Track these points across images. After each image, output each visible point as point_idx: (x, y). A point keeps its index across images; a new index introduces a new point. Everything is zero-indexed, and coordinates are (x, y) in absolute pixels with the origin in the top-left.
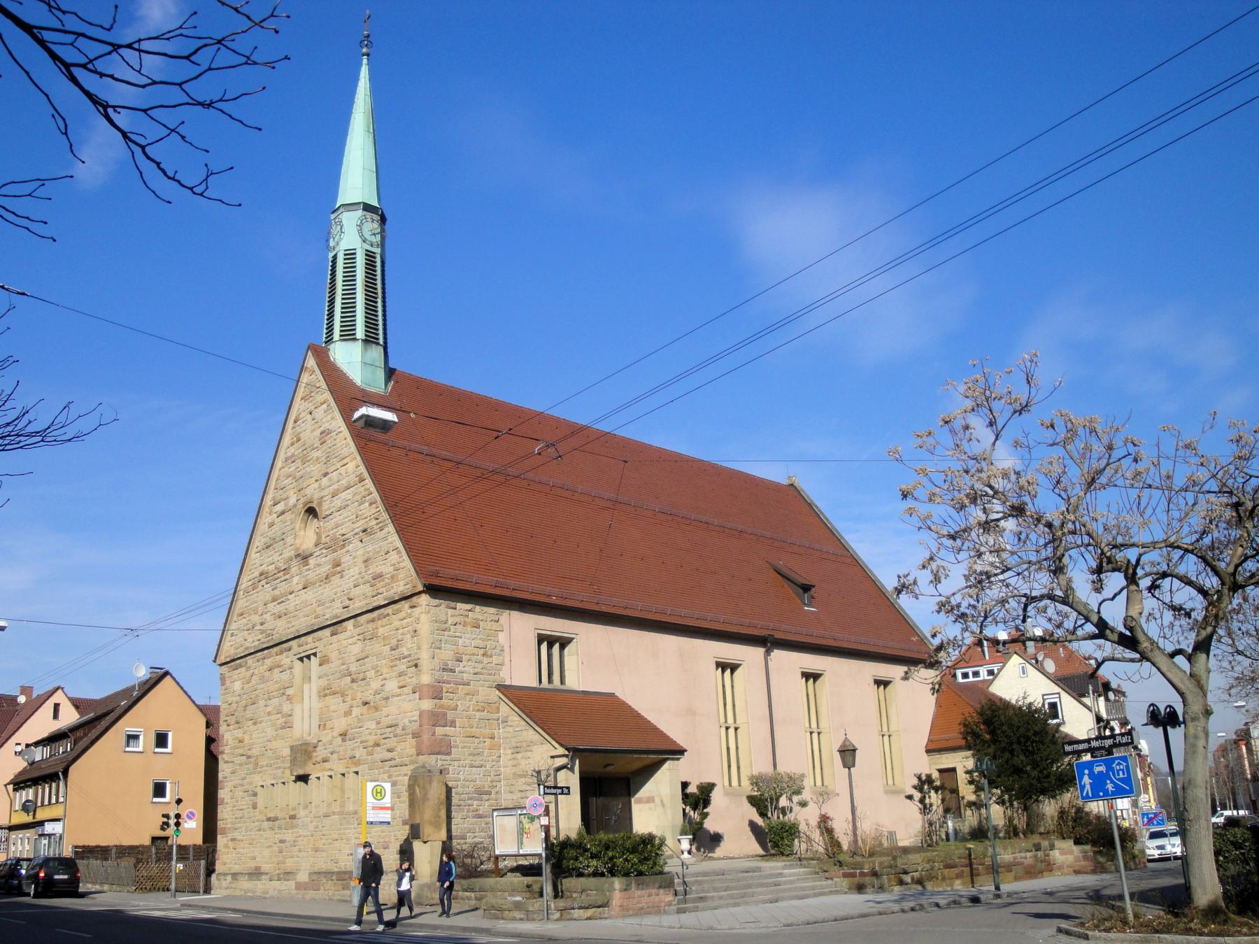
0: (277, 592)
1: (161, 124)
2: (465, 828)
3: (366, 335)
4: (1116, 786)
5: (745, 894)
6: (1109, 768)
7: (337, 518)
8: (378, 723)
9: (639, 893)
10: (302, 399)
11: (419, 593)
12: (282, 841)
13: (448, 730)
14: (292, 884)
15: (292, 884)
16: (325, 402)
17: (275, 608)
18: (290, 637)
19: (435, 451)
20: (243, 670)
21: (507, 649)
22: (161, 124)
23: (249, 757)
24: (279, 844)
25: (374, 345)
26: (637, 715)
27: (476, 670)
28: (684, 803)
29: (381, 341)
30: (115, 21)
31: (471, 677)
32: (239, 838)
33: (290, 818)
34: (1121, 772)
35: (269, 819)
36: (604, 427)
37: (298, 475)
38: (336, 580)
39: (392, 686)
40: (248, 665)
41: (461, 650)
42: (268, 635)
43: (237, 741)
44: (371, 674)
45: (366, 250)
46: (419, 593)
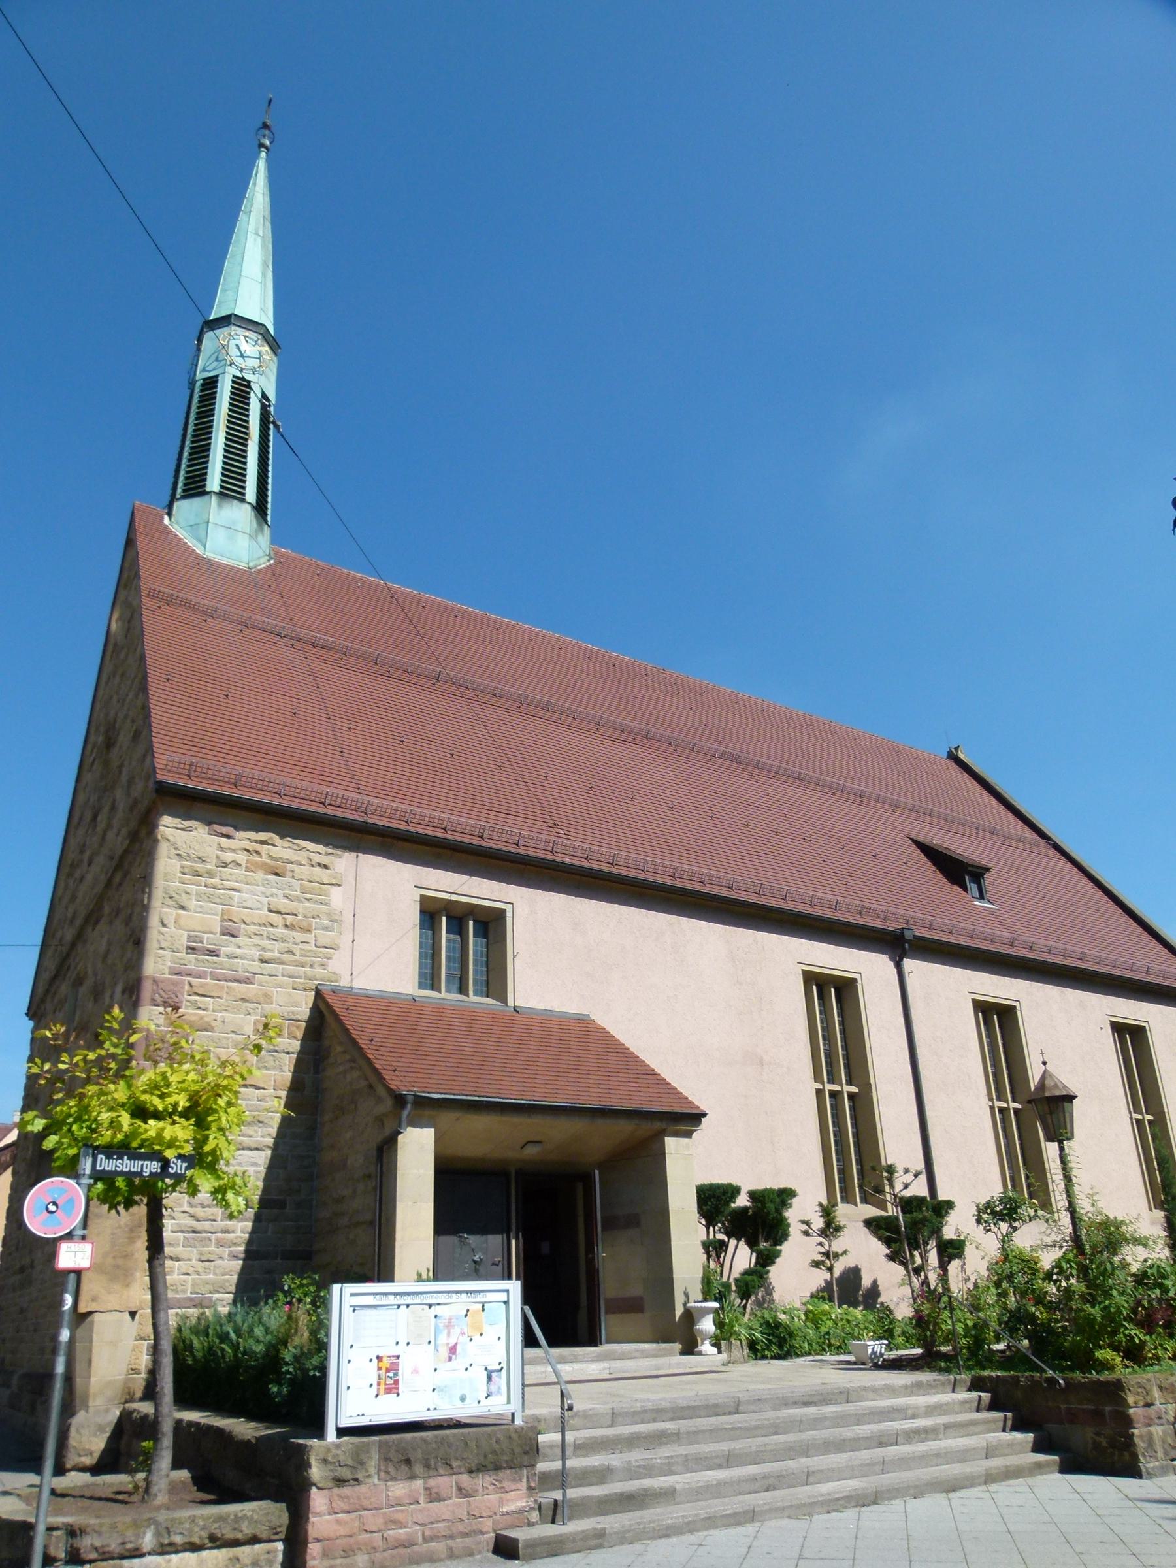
1: (284, 439)
3: (222, 487)
5: (780, 1477)
9: (399, 1489)
11: (1062, 1149)
21: (348, 918)
22: (284, 439)
25: (235, 502)
26: (622, 1051)
27: (267, 955)
28: (710, 1221)
29: (251, 494)
31: (256, 966)
41: (237, 913)
45: (234, 376)
46: (1062, 1149)
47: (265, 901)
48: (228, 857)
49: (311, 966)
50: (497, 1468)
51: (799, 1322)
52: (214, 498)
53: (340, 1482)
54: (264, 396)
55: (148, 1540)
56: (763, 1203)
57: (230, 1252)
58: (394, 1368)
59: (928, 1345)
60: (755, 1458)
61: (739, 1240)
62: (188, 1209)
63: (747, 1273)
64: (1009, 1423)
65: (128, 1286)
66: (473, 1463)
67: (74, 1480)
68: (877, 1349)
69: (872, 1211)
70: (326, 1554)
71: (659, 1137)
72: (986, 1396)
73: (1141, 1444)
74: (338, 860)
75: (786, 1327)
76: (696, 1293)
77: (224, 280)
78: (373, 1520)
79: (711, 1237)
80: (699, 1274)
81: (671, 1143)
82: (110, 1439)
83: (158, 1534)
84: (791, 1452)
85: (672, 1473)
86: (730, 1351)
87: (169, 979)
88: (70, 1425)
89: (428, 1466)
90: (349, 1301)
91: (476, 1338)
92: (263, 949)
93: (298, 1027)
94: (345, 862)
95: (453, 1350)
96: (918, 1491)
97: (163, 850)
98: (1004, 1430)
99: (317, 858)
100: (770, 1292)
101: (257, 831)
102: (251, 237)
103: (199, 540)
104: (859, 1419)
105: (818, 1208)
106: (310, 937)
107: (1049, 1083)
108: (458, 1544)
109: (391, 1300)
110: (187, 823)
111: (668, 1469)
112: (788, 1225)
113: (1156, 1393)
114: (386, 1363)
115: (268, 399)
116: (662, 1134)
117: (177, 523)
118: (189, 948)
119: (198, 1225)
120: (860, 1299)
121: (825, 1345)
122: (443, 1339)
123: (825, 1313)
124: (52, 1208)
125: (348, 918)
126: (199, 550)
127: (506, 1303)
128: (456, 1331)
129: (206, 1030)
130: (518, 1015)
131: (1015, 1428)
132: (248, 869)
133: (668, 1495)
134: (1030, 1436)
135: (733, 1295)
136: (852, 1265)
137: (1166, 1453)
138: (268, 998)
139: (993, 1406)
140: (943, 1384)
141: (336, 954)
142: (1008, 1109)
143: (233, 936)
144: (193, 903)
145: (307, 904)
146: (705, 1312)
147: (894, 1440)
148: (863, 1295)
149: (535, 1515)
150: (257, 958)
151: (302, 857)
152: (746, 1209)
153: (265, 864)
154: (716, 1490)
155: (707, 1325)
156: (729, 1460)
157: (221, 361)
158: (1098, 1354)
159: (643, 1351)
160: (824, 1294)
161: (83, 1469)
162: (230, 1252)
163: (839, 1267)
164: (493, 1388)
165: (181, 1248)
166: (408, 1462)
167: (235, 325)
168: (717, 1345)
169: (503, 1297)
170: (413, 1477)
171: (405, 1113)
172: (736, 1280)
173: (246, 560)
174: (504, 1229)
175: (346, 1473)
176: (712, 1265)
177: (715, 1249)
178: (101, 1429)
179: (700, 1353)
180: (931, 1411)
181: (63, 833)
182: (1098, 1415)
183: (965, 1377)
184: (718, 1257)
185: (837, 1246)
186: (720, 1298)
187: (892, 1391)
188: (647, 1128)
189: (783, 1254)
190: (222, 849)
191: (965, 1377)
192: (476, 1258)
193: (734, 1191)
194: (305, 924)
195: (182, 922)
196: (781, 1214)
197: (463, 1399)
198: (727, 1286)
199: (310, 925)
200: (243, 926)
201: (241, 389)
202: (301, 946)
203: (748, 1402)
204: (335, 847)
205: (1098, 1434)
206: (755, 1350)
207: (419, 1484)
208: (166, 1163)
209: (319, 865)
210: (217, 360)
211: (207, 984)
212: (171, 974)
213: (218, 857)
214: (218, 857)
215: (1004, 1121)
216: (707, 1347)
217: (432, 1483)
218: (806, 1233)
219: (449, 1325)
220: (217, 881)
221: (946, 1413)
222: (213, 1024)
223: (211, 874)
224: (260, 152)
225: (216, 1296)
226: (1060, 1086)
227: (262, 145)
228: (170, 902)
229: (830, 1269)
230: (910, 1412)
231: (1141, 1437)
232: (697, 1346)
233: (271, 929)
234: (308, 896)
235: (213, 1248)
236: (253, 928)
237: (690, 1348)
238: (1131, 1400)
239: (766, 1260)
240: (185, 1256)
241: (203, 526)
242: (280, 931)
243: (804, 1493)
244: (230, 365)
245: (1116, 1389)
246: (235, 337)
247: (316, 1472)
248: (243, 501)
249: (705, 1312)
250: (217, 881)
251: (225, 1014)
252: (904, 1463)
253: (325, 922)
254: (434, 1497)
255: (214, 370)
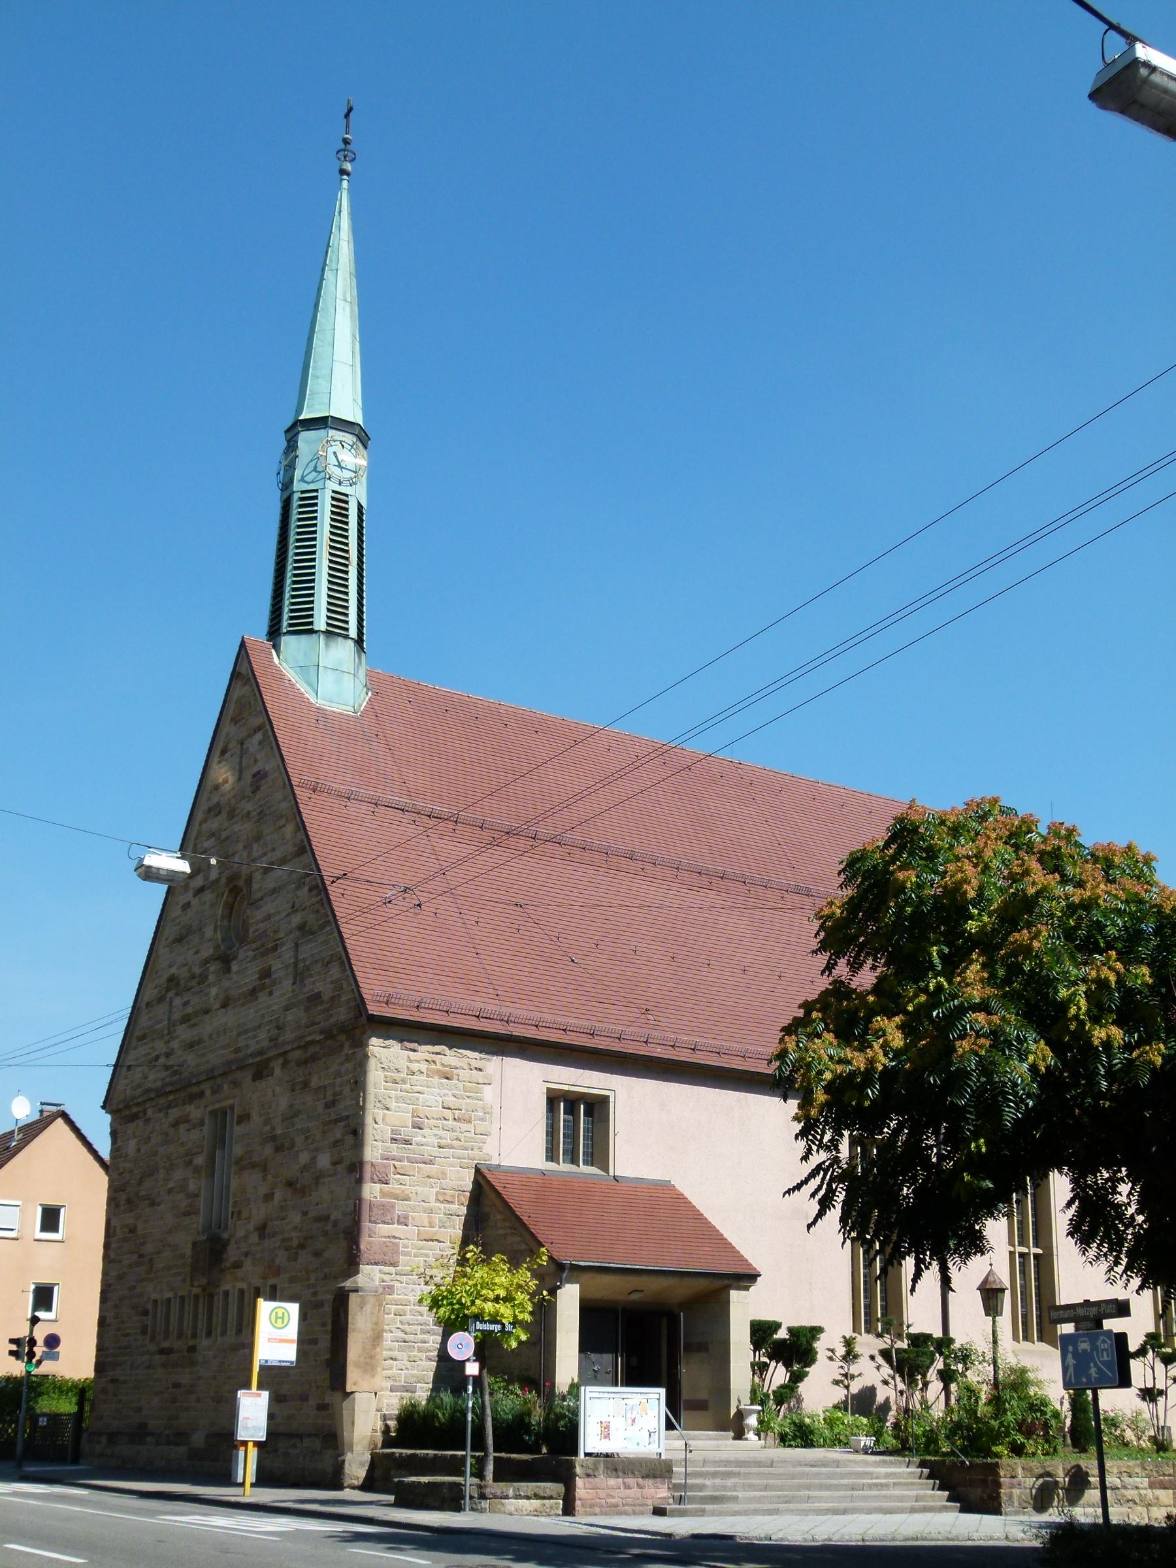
0: (189, 1010)
2: (413, 1376)
4: (1099, 1371)
5: (793, 1497)
6: (1094, 1347)
7: (269, 907)
8: (305, 1214)
9: (612, 1482)
10: (232, 720)
11: (994, 1322)
13: (396, 1229)
15: (182, 1450)
16: (259, 728)
17: (184, 1033)
19: (420, 804)
20: (140, 1122)
21: (496, 1110)
23: (141, 1256)
24: (171, 1390)
25: (340, 639)
26: (698, 1216)
27: (443, 1142)
29: (353, 633)
31: (435, 1151)
32: (122, 1378)
34: (1105, 1354)
35: (162, 1351)
36: (698, 747)
37: (224, 835)
38: (263, 997)
39: (324, 1161)
40: (148, 1117)
42: (176, 1073)
43: (126, 1230)
44: (299, 1140)
45: (334, 492)
47: (440, 1099)
48: (415, 1067)
49: (472, 1149)
50: (655, 1477)
51: (820, 1424)
52: (322, 637)
53: (588, 1476)
54: (359, 504)
55: (511, 1493)
56: (798, 1337)
57: (427, 1356)
58: (607, 1427)
59: (904, 1442)
60: (781, 1488)
61: (777, 1362)
62: (400, 1326)
63: (782, 1387)
64: (937, 1486)
65: (373, 1376)
66: (645, 1472)
67: (347, 1494)
68: (868, 1443)
69: (885, 1342)
70: (583, 1505)
71: (725, 1290)
72: (926, 1471)
73: (1004, 1498)
74: (488, 1063)
75: (808, 1427)
76: (746, 1399)
77: (314, 362)
78: (602, 1494)
79: (757, 1359)
80: (749, 1388)
81: (734, 1294)
82: (368, 1471)
83: (514, 1490)
84: (800, 1487)
85: (736, 1491)
86: (765, 1439)
87: (382, 1164)
88: (343, 1461)
89: (624, 1473)
90: (588, 1395)
91: (644, 1415)
92: (440, 1138)
93: (464, 1196)
94: (494, 1065)
95: (634, 1421)
96: (869, 1512)
97: (372, 1064)
98: (933, 1489)
99: (474, 1064)
100: (799, 1400)
101: (434, 1044)
102: (340, 304)
103: (310, 684)
104: (843, 1476)
105: (842, 1340)
106: (470, 1127)
107: (991, 1279)
108: (637, 1509)
109: (606, 1395)
110: (388, 1042)
111: (734, 1488)
112: (816, 1353)
113: (1020, 1471)
114: (604, 1425)
115: (362, 507)
116: (728, 1288)
117: (286, 661)
118: (392, 1139)
119: (408, 1337)
120: (874, 1412)
121: (837, 1442)
122: (629, 1415)
123: (838, 1419)
124: (460, 1346)
125: (496, 1110)
126: (313, 700)
127: (659, 1399)
128: (635, 1412)
129: (406, 1200)
130: (617, 1184)
131: (939, 1489)
132: (428, 1076)
133: (735, 1499)
134: (947, 1493)
135: (771, 1402)
136: (869, 1385)
137: (1020, 1504)
138: (444, 1175)
139: (929, 1477)
140: (901, 1462)
141: (488, 1139)
142: (1028, 1254)
143: (420, 1129)
144: (393, 1105)
145: (468, 1101)
146: (751, 1412)
147: (862, 1487)
148: (876, 1409)
149: (671, 1501)
150: (436, 1144)
151: (463, 1063)
152: (784, 1340)
153: (439, 1071)
154: (759, 1500)
155: (752, 1421)
156: (766, 1488)
157: (320, 472)
158: (994, 1449)
159: (707, 1435)
160: (842, 1406)
161: (353, 1488)
162: (427, 1356)
163: (855, 1387)
164: (652, 1440)
165: (396, 1352)
166: (616, 1470)
167: (331, 428)
168: (758, 1435)
169: (657, 1396)
170: (618, 1477)
171: (565, 1275)
172: (774, 1392)
173: (352, 703)
174: (614, 1350)
175: (590, 1472)
176: (757, 1379)
177: (759, 1368)
178: (362, 1464)
179: (747, 1439)
180: (888, 1475)
181: (150, 941)
182: (984, 1482)
183: (916, 1460)
184: (761, 1375)
185: (854, 1369)
186: (762, 1403)
187: (866, 1463)
188: (718, 1284)
189: (810, 1375)
190: (410, 1061)
191: (916, 1460)
192: (596, 1369)
193: (776, 1326)
194: (467, 1117)
195: (388, 1120)
196: (811, 1345)
197: (638, 1444)
198: (767, 1395)
199: (471, 1118)
200: (426, 1120)
201: (340, 500)
202: (465, 1134)
203: (778, 1462)
204: (487, 1053)
205: (983, 1492)
206: (783, 1439)
207: (620, 1480)
208: (503, 1325)
209: (476, 1068)
210: (315, 470)
211: (405, 1166)
212: (383, 1159)
213: (408, 1068)
214: (408, 1068)
215: (1024, 1266)
216: (751, 1435)
217: (626, 1480)
218: (831, 1359)
219: (632, 1409)
220: (408, 1086)
221: (898, 1478)
222: (411, 1195)
223: (404, 1081)
224: (342, 180)
225: (419, 1385)
226: (998, 1281)
227: (343, 172)
228: (378, 1105)
229: (847, 1387)
230: (874, 1476)
231: (1005, 1494)
232: (744, 1434)
233: (445, 1122)
234: (469, 1094)
235: (416, 1353)
236: (432, 1122)
237: (739, 1435)
238: (1002, 1473)
239: (796, 1378)
240: (399, 1357)
241: (313, 670)
242: (451, 1123)
243: (804, 1506)
244: (329, 479)
245: (993, 1469)
246: (333, 443)
247: (578, 1470)
248: (347, 637)
249: (751, 1412)
250: (408, 1086)
251: (417, 1188)
252: (864, 1498)
253: (481, 1114)
254: (627, 1487)
255: (313, 482)
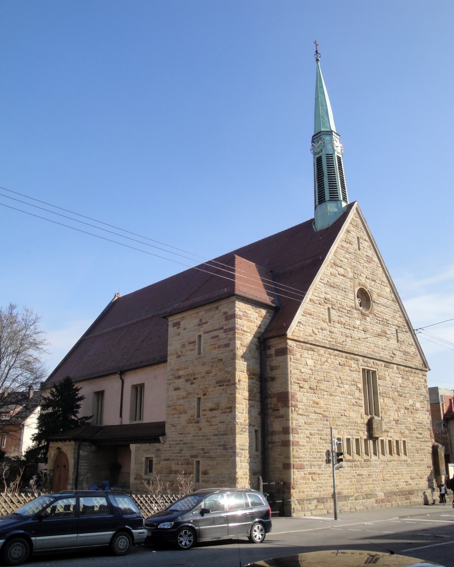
12: (359, 475)
14: (373, 500)
15: (373, 500)
18: (360, 354)
30: (317, 45)
33: (364, 461)
